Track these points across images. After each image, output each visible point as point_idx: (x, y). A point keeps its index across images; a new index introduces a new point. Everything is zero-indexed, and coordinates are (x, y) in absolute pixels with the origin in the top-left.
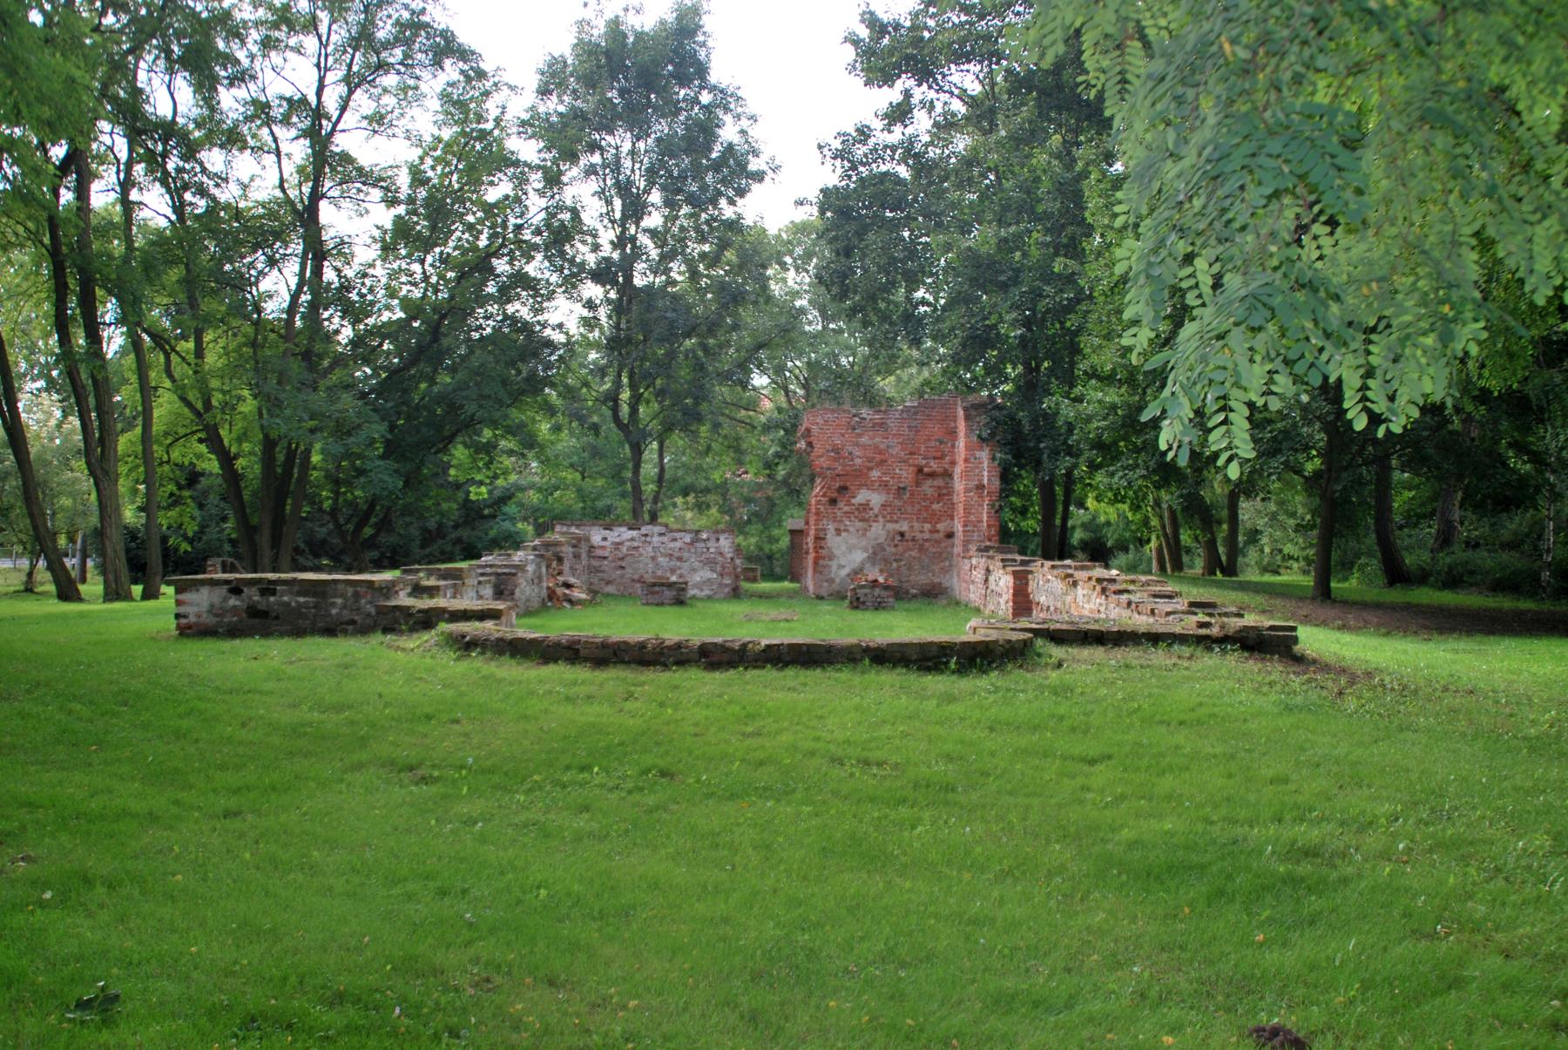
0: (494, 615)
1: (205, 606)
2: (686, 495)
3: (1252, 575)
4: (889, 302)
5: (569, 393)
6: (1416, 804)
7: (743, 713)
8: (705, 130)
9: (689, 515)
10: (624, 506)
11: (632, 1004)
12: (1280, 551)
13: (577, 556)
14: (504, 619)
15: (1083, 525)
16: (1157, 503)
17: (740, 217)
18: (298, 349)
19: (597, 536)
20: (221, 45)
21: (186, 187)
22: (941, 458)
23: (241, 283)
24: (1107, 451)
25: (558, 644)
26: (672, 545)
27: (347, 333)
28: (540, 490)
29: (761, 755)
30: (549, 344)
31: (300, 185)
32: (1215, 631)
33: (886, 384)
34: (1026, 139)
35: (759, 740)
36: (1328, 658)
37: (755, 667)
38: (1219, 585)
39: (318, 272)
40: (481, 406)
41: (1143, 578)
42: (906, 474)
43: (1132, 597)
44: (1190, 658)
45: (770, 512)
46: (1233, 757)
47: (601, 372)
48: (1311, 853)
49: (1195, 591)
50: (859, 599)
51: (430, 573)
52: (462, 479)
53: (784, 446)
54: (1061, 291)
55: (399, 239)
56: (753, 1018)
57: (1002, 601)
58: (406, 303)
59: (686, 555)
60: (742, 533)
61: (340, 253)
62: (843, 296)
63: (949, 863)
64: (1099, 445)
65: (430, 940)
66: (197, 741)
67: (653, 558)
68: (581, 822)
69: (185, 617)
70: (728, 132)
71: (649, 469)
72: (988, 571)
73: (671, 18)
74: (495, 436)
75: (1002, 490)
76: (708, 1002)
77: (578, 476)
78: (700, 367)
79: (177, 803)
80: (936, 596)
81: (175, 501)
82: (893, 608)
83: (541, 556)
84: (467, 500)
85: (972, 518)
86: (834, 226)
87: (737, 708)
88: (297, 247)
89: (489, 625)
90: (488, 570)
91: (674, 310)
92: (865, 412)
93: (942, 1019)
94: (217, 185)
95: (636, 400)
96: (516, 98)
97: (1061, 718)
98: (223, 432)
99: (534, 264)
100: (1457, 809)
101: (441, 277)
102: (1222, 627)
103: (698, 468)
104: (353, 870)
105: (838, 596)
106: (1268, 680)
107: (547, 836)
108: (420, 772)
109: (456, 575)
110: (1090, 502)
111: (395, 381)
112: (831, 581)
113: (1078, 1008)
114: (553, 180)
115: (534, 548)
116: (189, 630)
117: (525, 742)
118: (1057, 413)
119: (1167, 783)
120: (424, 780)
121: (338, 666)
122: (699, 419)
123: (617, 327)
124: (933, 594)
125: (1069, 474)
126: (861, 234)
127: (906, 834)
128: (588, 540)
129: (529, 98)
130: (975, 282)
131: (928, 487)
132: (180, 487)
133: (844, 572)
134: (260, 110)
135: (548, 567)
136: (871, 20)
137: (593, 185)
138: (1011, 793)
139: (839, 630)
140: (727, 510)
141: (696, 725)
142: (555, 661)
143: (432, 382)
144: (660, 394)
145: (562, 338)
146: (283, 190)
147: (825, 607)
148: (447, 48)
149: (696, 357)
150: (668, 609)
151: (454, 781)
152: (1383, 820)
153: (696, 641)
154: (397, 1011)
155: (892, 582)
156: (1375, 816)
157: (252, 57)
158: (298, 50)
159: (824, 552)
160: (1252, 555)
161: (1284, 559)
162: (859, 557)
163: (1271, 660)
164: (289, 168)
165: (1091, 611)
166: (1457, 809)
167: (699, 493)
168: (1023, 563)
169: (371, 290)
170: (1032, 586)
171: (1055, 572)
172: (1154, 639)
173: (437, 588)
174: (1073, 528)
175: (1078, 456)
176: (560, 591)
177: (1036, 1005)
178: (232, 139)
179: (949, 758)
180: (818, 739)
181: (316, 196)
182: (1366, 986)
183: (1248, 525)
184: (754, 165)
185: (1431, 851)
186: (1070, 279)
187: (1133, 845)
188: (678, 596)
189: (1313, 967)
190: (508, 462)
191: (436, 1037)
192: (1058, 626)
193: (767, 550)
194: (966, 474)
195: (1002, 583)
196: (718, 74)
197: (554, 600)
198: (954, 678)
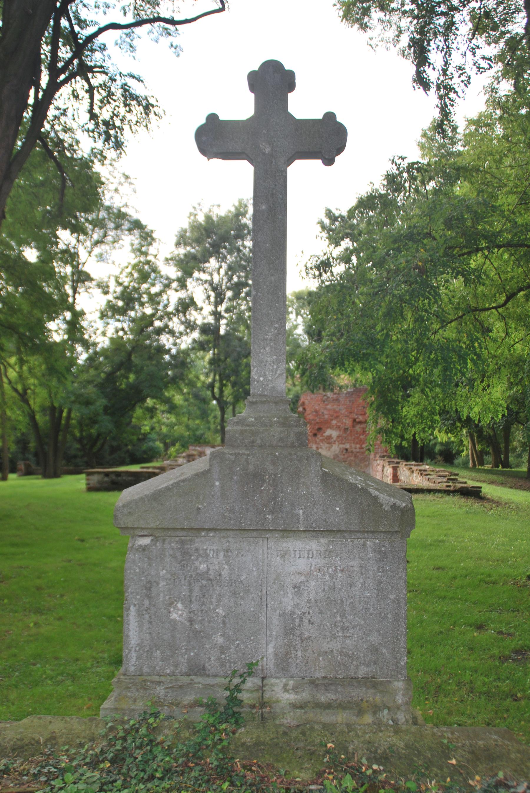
28: (167, 426)
42: (348, 422)
55: (111, 311)
72: (383, 467)
73: (233, 210)
95: (222, 386)
96: (165, 250)
102: (454, 487)
114: (183, 285)
116: (91, 489)
131: (358, 428)
136: (329, 214)
172: (429, 491)
195: (388, 471)
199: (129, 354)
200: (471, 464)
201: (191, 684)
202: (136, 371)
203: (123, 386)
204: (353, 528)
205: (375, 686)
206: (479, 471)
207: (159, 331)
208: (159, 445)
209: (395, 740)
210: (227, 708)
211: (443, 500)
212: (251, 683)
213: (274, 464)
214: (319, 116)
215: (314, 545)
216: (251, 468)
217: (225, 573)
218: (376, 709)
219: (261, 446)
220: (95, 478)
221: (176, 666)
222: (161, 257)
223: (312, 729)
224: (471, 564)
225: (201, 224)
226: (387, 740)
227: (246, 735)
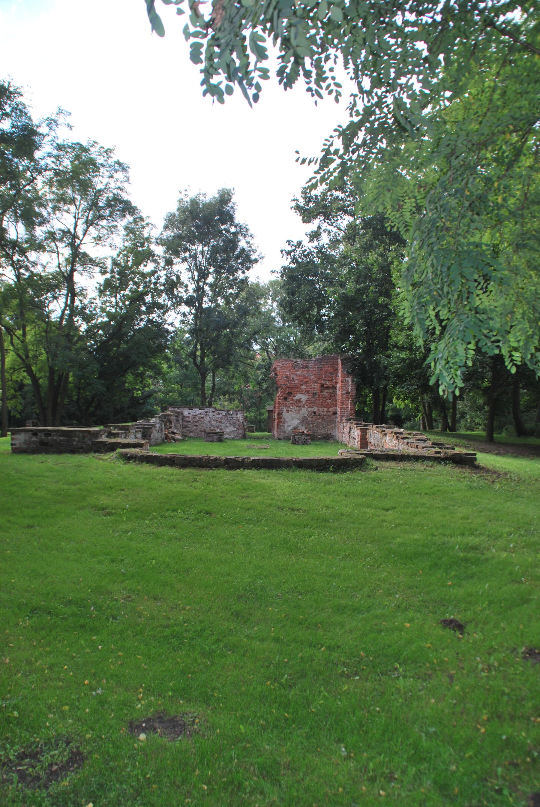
0: (140, 445)
1: (23, 440)
2: (224, 395)
3: (463, 432)
4: (310, 315)
5: (176, 352)
6: (519, 528)
7: (242, 488)
8: (232, 243)
9: (226, 403)
10: (198, 400)
11: (187, 608)
12: (474, 421)
13: (177, 421)
14: (144, 447)
15: (392, 409)
16: (422, 399)
17: (246, 278)
18: (62, 335)
19: (186, 412)
20: (37, 209)
21: (21, 267)
22: (332, 380)
23: (42, 306)
24: (400, 378)
25: (166, 458)
26: (218, 416)
27: (84, 327)
28: (163, 393)
29: (248, 506)
30: (168, 332)
31: (66, 266)
32: (442, 455)
33: (310, 349)
34: (367, 248)
35: (249, 500)
36: (489, 467)
37: (248, 469)
38: (448, 435)
39: (73, 301)
40: (138, 357)
41: (414, 432)
43: (409, 440)
44: (431, 467)
45: (260, 403)
46: (446, 508)
47: (188, 343)
48: (475, 548)
49: (437, 438)
50: (296, 439)
51: (115, 428)
52: (130, 388)
53: (265, 376)
54: (382, 312)
55: (108, 287)
56: (237, 614)
57: (356, 441)
58: (109, 314)
59: (223, 420)
60: (248, 411)
61: (82, 294)
62: (291, 312)
63: (323, 552)
64: (397, 376)
65: (107, 580)
66: (18, 496)
67: (210, 422)
68: (172, 533)
69: (15, 445)
70: (242, 244)
71: (209, 384)
72: (350, 428)
74: (144, 370)
75: (357, 394)
76: (219, 607)
77: (179, 387)
78: (230, 341)
79: (9, 521)
80: (329, 439)
81: (14, 397)
82: (310, 444)
83: (162, 421)
84: (133, 397)
85: (344, 406)
86: (287, 283)
87: (239, 486)
88: (64, 292)
89: (138, 450)
90: (140, 426)
91: (219, 317)
92: (299, 361)
93: (316, 616)
94: (33, 266)
95: (203, 355)
96: (156, 228)
97: (376, 491)
98: (34, 368)
99: (162, 298)
100: (536, 530)
101: (124, 303)
102: (445, 453)
103: (230, 384)
104: (78, 551)
105: (287, 439)
106: (463, 475)
107: (157, 538)
108: (107, 511)
109: (127, 428)
110: (395, 400)
111: (103, 347)
112: (285, 432)
113: (371, 612)
114: (169, 263)
115: (160, 417)
116: (17, 450)
117: (151, 499)
118: (380, 362)
119: (417, 520)
120: (108, 514)
121: (76, 466)
122: (230, 363)
123: (196, 324)
124: (328, 438)
125: (385, 387)
126: (299, 286)
127: (307, 539)
128: (182, 414)
129: (161, 229)
130: (345, 306)
131: (326, 393)
132: (16, 391)
133: (290, 428)
134: (51, 236)
135: (165, 425)
137: (186, 265)
138: (352, 523)
139: (286, 453)
140: (242, 401)
141: (222, 493)
142: (165, 465)
143: (119, 347)
144: (213, 353)
145: (173, 329)
146: (59, 267)
147: (282, 443)
148: (128, 208)
149: (228, 337)
150: (215, 443)
151: (121, 515)
152: (505, 535)
153: (224, 457)
154: (92, 608)
155: (310, 433)
156: (502, 533)
157: (49, 214)
158: (68, 211)
159: (282, 420)
160: (463, 422)
161: (475, 425)
162: (296, 422)
163: (465, 468)
164: (62, 259)
165: (392, 446)
166: (536, 530)
167: (231, 395)
168: (365, 425)
169: (95, 309)
170: (368, 436)
171: (378, 429)
172: (417, 458)
173: (118, 434)
174: (388, 410)
175: (389, 380)
176: (170, 435)
177: (354, 610)
178: (40, 247)
179: (327, 508)
180: (273, 499)
181: (73, 270)
182: (490, 603)
183: (461, 410)
184: (253, 257)
185: (523, 547)
186: (385, 306)
187: (401, 545)
188: (219, 438)
189: (470, 595)
190: (150, 381)
191: (107, 619)
192: (377, 452)
193: (258, 418)
196: (238, 219)
197: (167, 439)
198: (331, 474)
211: (433, 470)
225: (187, 208)
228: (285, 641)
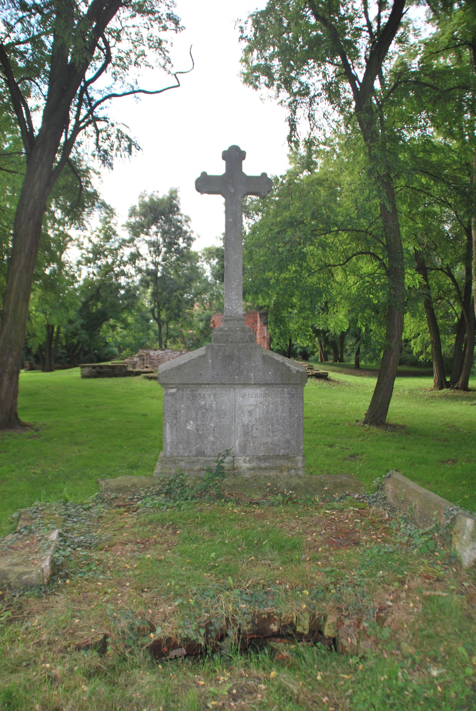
19: (152, 353)
73: (168, 195)
95: (160, 310)
116: (84, 377)
122: (179, 316)
144: (168, 309)
194: (260, 333)
199: (98, 290)
200: (319, 360)
201: (198, 460)
202: (103, 300)
203: (94, 311)
204: (278, 382)
205: (288, 459)
206: (325, 364)
207: (117, 276)
208: (116, 350)
209: (299, 481)
210: (217, 470)
212: (228, 459)
213: (238, 351)
214: (259, 175)
215: (259, 391)
216: (227, 353)
217: (214, 406)
218: (289, 469)
219: (231, 342)
220: (87, 370)
221: (190, 452)
222: (119, 225)
223: (259, 478)
224: (324, 415)
225: (146, 203)
226: (295, 481)
227: (228, 481)
228: (221, 595)
